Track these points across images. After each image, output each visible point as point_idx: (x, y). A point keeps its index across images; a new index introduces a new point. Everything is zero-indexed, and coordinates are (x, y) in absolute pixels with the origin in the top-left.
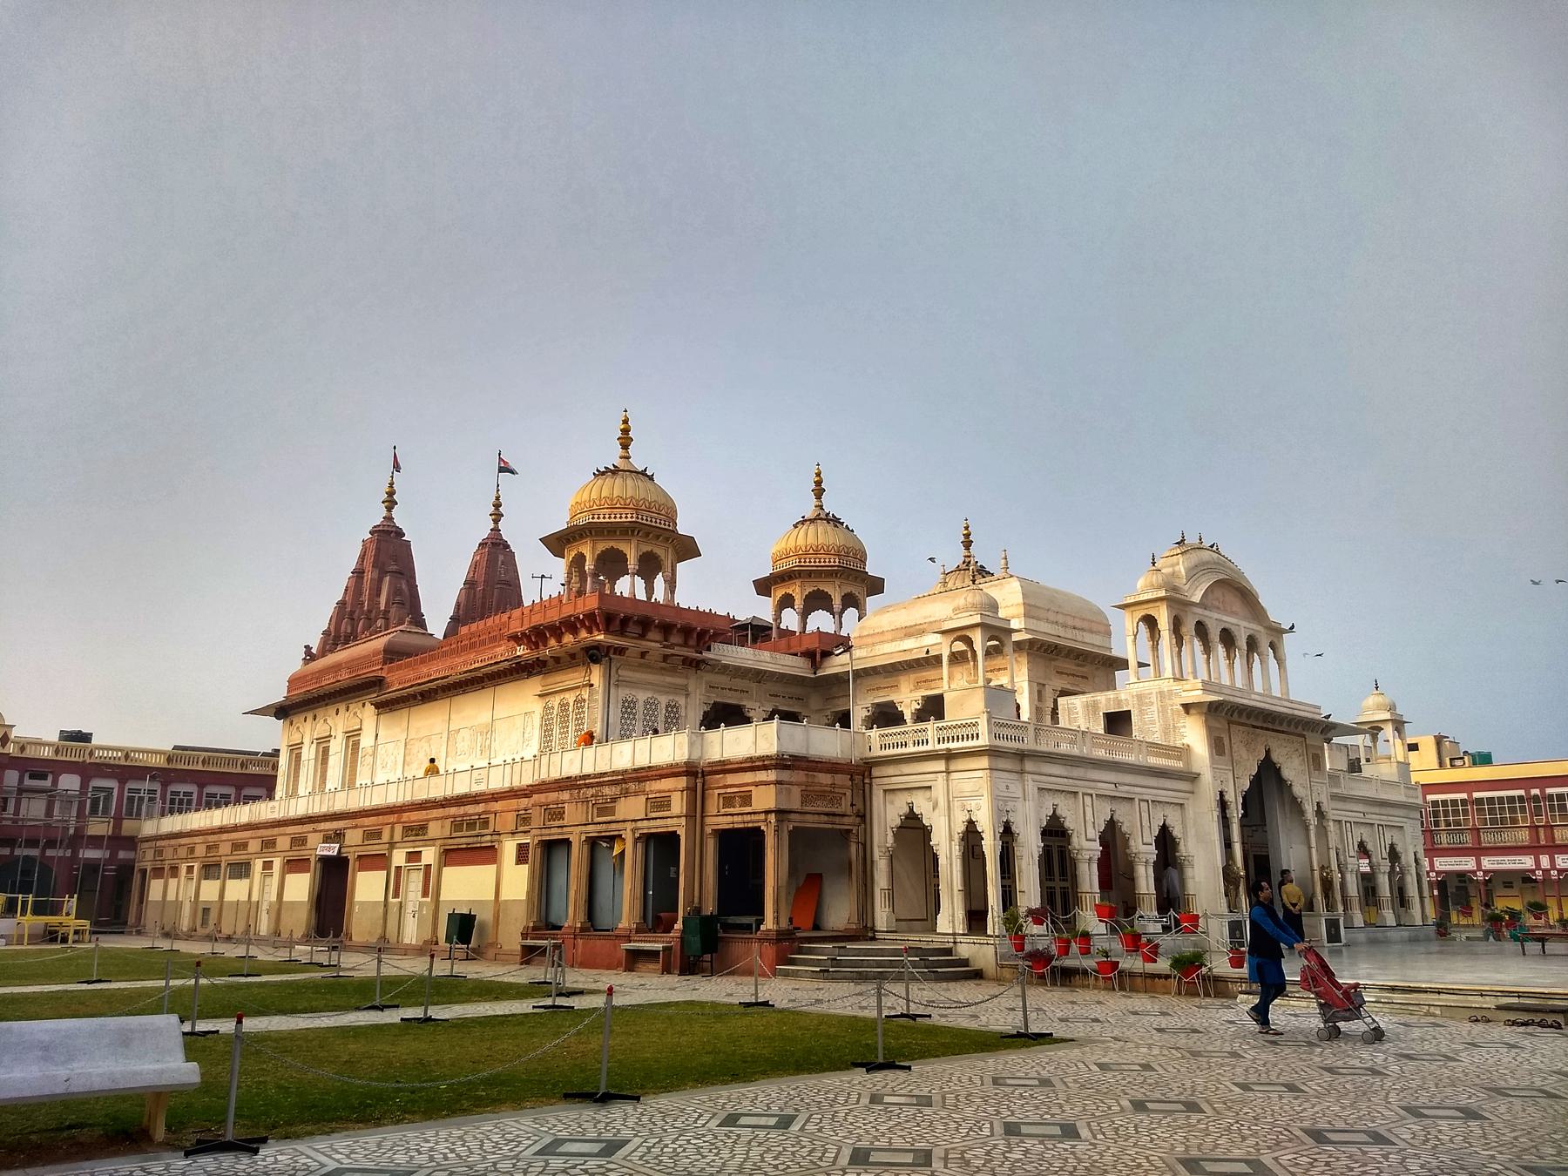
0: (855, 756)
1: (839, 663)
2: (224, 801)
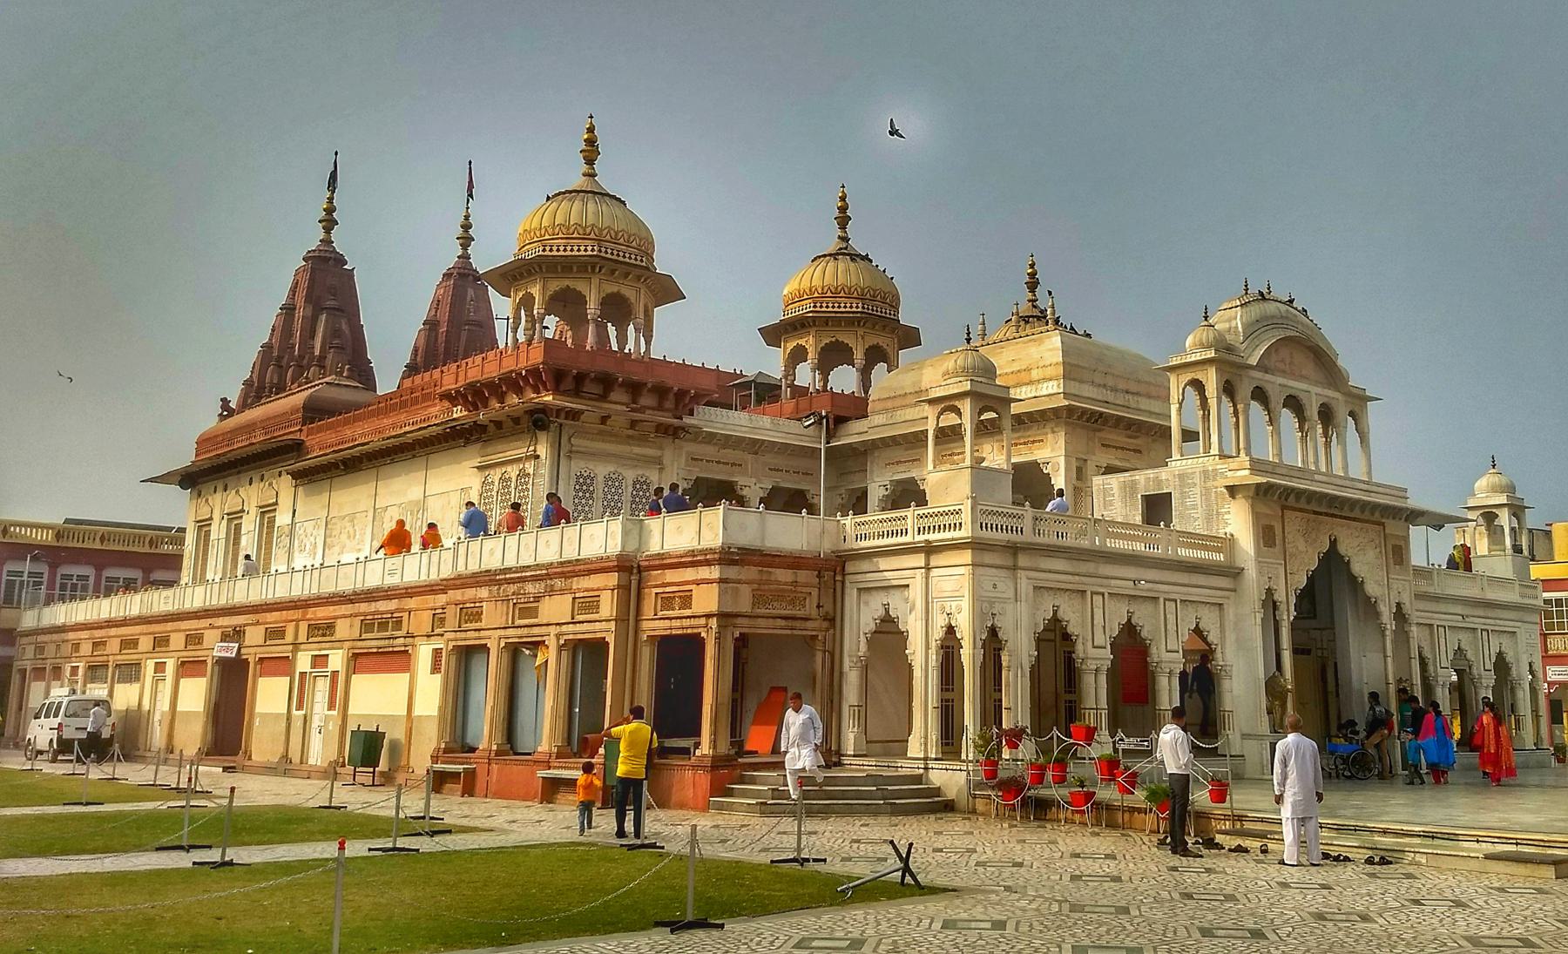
0: (826, 547)
1: (855, 433)
2: (129, 586)
